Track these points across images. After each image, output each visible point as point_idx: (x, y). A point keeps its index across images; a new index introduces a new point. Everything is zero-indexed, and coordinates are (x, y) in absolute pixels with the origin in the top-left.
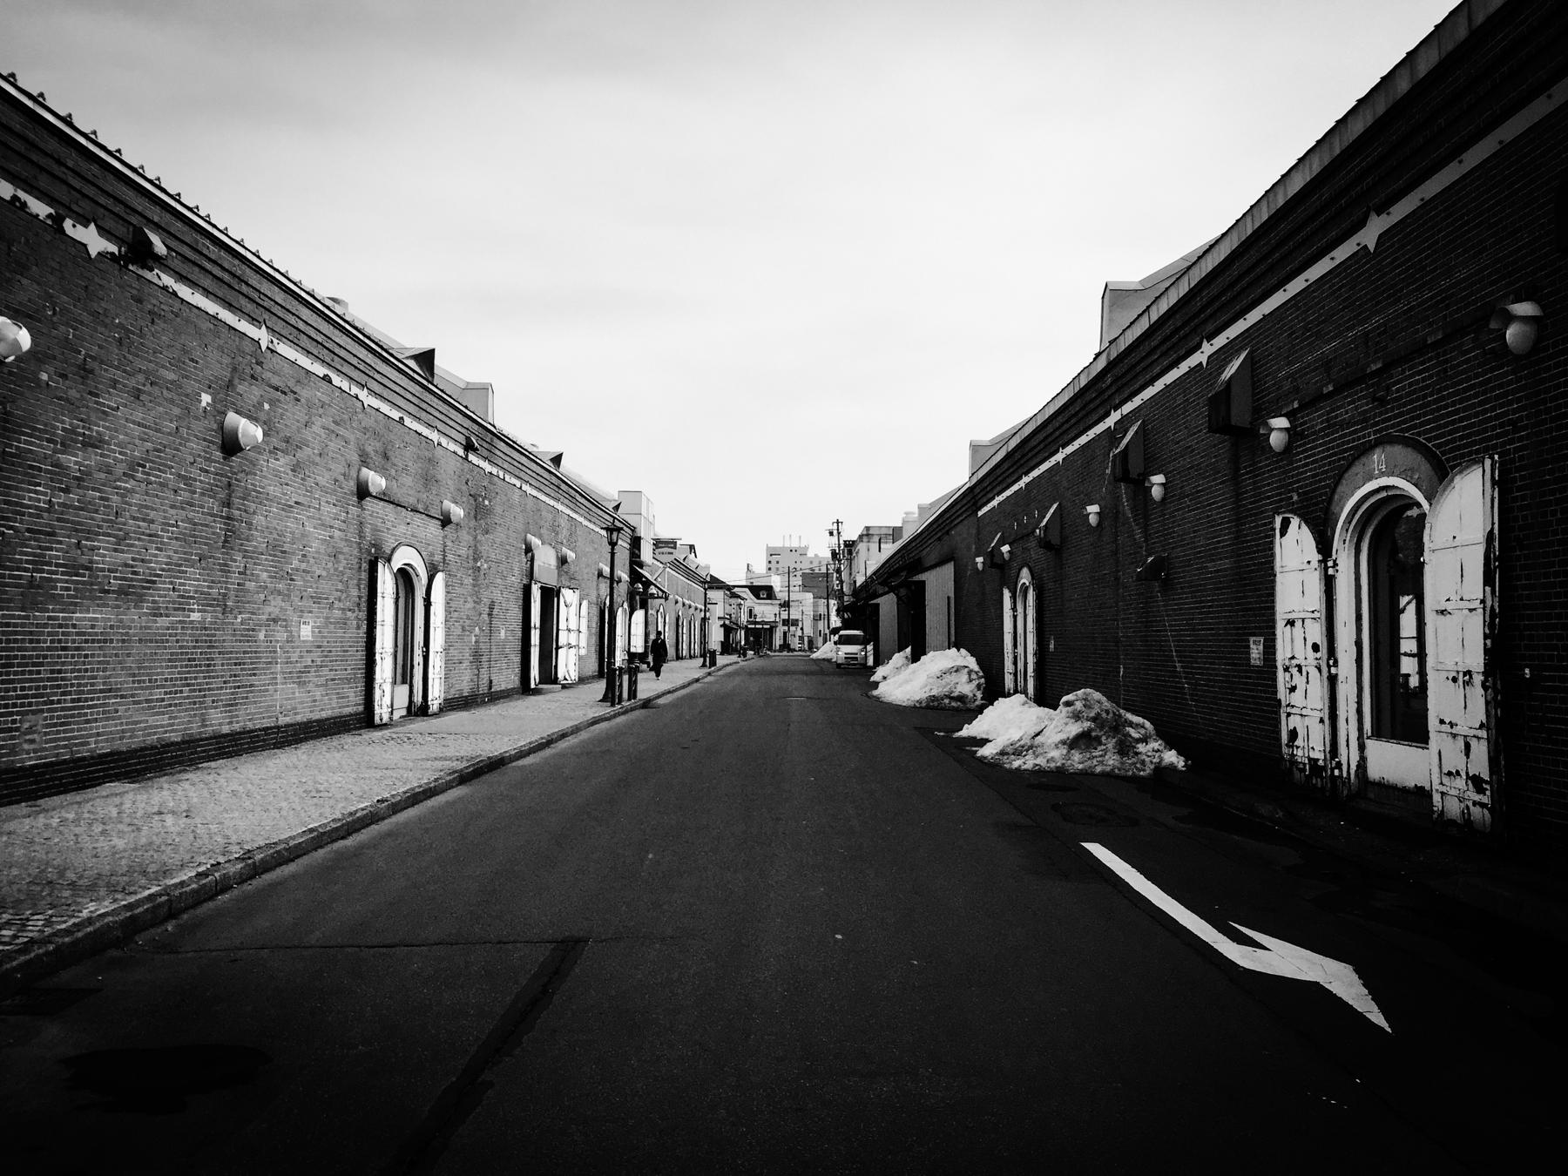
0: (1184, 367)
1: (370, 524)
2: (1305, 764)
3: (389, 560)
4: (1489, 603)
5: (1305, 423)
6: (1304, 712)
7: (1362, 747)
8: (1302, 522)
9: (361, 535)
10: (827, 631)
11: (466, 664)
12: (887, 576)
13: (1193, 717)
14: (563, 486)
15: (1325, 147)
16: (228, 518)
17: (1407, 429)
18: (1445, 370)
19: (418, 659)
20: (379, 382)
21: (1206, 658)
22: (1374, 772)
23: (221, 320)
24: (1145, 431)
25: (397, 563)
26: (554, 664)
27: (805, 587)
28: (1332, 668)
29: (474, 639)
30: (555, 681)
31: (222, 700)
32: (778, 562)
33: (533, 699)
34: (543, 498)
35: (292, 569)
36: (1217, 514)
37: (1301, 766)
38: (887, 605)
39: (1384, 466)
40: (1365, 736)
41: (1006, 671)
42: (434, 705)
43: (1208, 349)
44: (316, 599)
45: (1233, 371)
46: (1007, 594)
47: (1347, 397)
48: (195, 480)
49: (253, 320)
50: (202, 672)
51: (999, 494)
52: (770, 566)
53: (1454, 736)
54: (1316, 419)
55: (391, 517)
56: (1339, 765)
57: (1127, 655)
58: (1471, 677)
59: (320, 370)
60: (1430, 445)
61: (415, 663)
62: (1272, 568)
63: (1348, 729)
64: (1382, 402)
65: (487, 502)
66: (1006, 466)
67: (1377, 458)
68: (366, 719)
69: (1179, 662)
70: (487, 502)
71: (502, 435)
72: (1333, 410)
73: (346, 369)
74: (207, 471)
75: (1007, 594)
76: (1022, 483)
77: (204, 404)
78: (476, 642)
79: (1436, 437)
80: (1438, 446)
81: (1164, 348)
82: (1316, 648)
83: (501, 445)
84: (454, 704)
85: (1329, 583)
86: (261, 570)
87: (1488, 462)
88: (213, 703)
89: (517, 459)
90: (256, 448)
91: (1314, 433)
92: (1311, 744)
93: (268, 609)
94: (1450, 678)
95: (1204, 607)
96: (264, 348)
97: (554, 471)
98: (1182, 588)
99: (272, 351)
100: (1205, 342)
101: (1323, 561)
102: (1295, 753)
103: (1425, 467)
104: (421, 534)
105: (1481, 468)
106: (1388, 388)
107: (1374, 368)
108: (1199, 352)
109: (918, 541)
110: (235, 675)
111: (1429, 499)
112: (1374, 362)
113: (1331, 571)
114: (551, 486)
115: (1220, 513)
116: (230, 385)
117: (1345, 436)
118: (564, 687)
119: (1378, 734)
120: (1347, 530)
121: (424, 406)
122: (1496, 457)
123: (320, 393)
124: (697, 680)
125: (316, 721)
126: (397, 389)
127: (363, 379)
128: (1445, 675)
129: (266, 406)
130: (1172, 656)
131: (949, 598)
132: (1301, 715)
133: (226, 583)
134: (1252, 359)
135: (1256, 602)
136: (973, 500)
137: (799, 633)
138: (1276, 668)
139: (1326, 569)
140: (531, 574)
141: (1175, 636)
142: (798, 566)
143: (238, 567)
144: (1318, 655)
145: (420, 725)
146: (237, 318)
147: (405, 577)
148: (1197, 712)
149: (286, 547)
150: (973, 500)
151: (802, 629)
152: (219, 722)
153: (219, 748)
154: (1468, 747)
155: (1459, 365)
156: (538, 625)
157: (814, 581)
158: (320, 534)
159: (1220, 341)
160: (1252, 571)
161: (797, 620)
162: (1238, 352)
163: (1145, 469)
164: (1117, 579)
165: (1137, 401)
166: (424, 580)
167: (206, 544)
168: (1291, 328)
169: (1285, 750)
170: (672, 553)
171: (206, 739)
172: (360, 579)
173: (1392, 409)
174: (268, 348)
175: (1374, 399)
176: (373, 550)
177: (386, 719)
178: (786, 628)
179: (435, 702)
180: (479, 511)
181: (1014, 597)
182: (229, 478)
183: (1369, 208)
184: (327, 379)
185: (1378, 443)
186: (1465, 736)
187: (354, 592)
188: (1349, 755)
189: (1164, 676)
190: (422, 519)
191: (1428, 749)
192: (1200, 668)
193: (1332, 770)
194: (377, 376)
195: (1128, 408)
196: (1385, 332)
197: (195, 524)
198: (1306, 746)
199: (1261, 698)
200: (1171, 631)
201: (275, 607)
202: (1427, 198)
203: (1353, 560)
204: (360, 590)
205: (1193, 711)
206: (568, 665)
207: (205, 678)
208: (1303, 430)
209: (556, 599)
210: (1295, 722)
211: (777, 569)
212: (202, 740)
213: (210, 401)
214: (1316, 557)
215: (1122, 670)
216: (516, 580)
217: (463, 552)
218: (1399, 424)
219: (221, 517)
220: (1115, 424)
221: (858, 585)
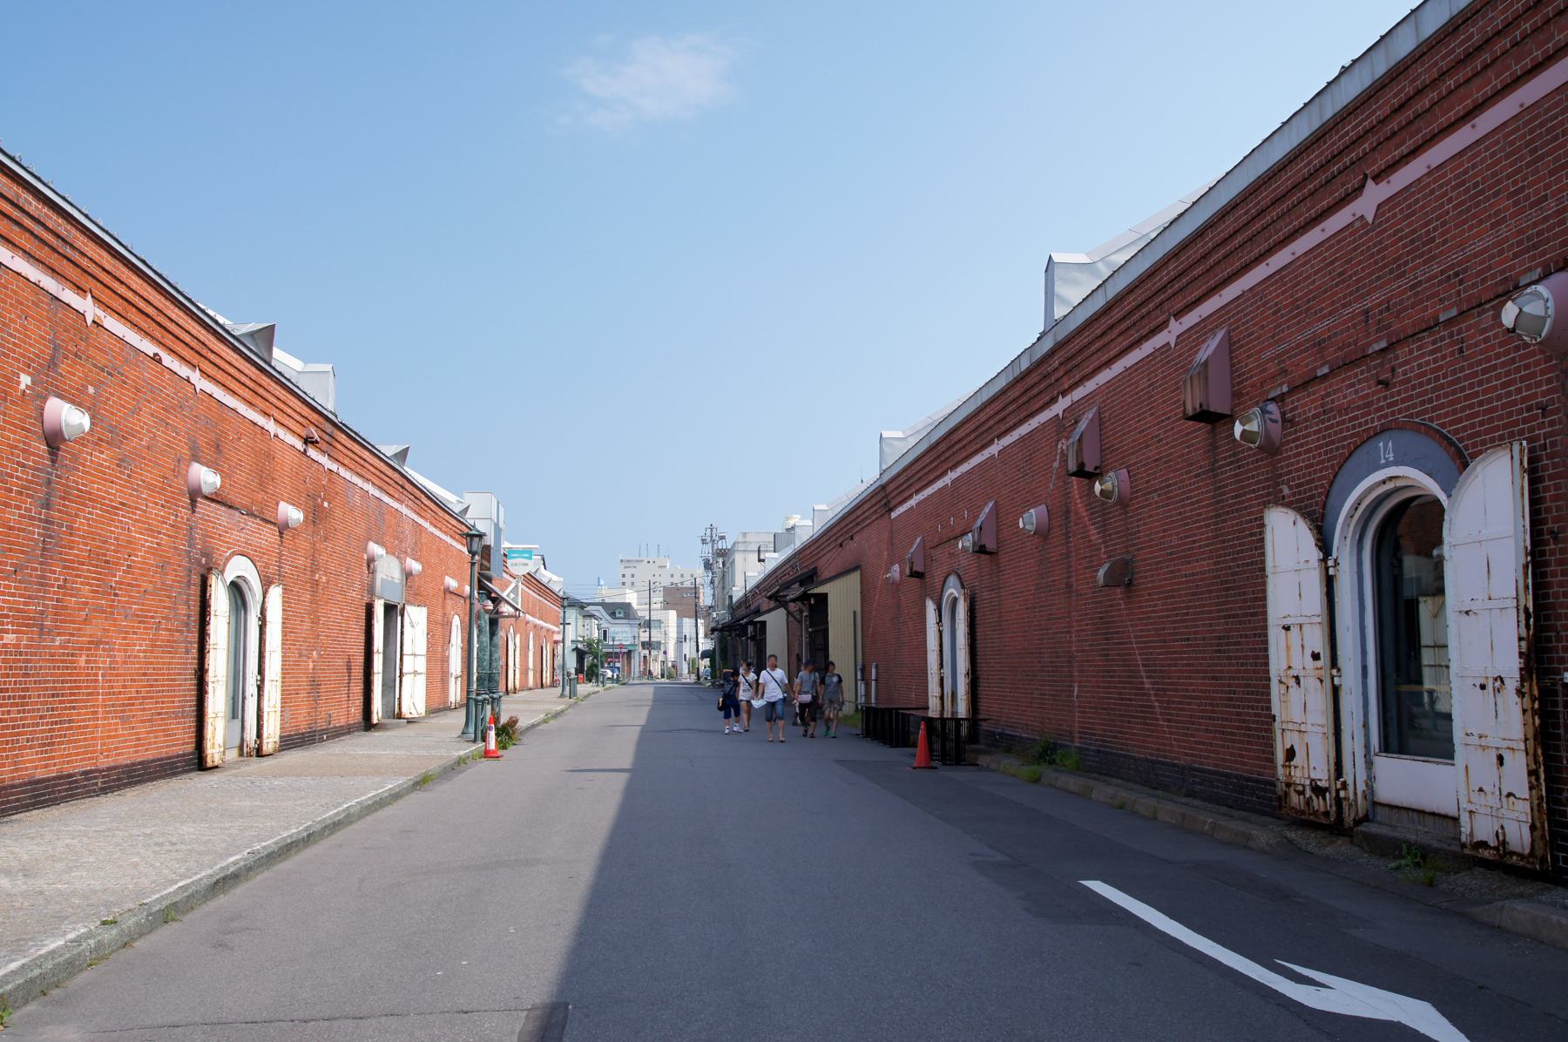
0: (1148, 348)
1: (201, 529)
2: (1304, 786)
3: (222, 572)
4: (1522, 603)
5: (1295, 408)
6: (1303, 728)
7: (1369, 764)
8: (1298, 517)
9: (191, 541)
10: (694, 655)
11: (303, 694)
12: (775, 589)
13: (1167, 738)
14: (408, 486)
15: (1314, 108)
16: (46, 522)
17: (1418, 414)
18: (1461, 351)
19: (251, 689)
20: (212, 362)
21: (1180, 671)
22: (1385, 793)
23: (42, 289)
24: (1100, 419)
25: (230, 575)
26: (397, 696)
27: (667, 605)
28: (1335, 679)
29: (311, 665)
30: (400, 716)
31: (38, 739)
32: (633, 576)
33: (375, 735)
34: (386, 499)
35: (116, 582)
36: (1191, 510)
37: (1300, 788)
38: (776, 623)
39: (1392, 455)
40: (1372, 753)
41: (930, 694)
42: (270, 743)
43: (1176, 328)
44: (141, 619)
45: (1210, 351)
46: (930, 607)
47: (1343, 381)
48: (11, 476)
49: (80, 290)
50: (16, 705)
51: (917, 492)
52: (624, 580)
53: (1484, 748)
54: (1305, 405)
55: (224, 520)
57: (1082, 671)
58: (1502, 682)
59: (149, 348)
60: (1444, 431)
61: (248, 694)
62: (1263, 569)
63: (1353, 745)
64: (1386, 384)
65: (326, 504)
66: (927, 460)
67: (1385, 447)
68: (199, 762)
69: (1148, 677)
70: (326, 504)
71: (344, 425)
72: (1328, 395)
73: (179, 348)
74: (23, 466)
75: (930, 607)
76: (948, 479)
77: (23, 387)
78: (314, 669)
79: (1452, 423)
80: (1456, 432)
81: (1123, 326)
82: (1316, 657)
83: (342, 438)
84: (289, 742)
85: (1329, 582)
86: (82, 583)
87: (1516, 447)
88: (28, 742)
89: (359, 453)
90: (82, 440)
91: (1306, 420)
92: (1314, 765)
93: (88, 630)
94: (1478, 685)
95: (1177, 615)
96: (89, 322)
97: (397, 467)
98: (1149, 594)
99: (99, 325)
100: (1172, 320)
101: (1324, 560)
102: (1292, 774)
103: (1441, 455)
104: (254, 540)
105: (1509, 456)
106: (1393, 370)
107: (1377, 347)
108: (1166, 330)
109: (813, 548)
110: (53, 709)
111: (1448, 490)
112: (1377, 340)
113: (1331, 571)
114: (396, 486)
115: (1196, 509)
116: (52, 364)
117: (1343, 422)
118: (410, 721)
119: (1386, 748)
120: (1349, 525)
121: (261, 391)
122: (1524, 443)
123: (148, 372)
124: (557, 715)
125: (141, 763)
126: (232, 371)
127: (195, 359)
128: (1470, 682)
129: (91, 390)
130: (1139, 671)
131: (855, 612)
132: (1300, 731)
133: (44, 598)
134: (1230, 338)
135: (1240, 608)
136: (885, 500)
137: (661, 657)
138: (1269, 679)
139: (1327, 569)
140: (371, 590)
141: (1142, 648)
142: (657, 579)
143: (57, 580)
144: (1319, 663)
145: (256, 764)
146: (61, 287)
147: (237, 590)
148: (1170, 733)
149: (110, 556)
150: (885, 500)
151: (665, 653)
152: (35, 766)
153: (35, 796)
154: (1500, 759)
155: (1476, 345)
156: (381, 650)
157: (681, 599)
158: (147, 541)
159: (1191, 319)
160: (1236, 573)
161: (659, 643)
162: (1213, 331)
163: (1102, 462)
164: (1069, 586)
165: (1090, 386)
166: (259, 597)
167: (23, 552)
168: (1276, 305)
169: (1280, 771)
170: (526, 565)
171: (20, 785)
172: (189, 595)
173: (1399, 393)
174: (94, 322)
175: (1380, 382)
176: (204, 560)
177: (217, 761)
178: (647, 652)
179: (271, 740)
180: (316, 515)
181: (939, 610)
182: (48, 473)
183: (1366, 177)
184: (156, 359)
185: (1384, 430)
186: (1497, 748)
187: (183, 610)
188: (1354, 771)
189: (1129, 694)
190: (257, 524)
191: (1453, 765)
192: (1173, 684)
193: (1337, 791)
194: (212, 357)
195: (1078, 394)
196: (1388, 309)
197: (11, 528)
198: (1306, 766)
199: (1247, 715)
200: (1137, 643)
201: (95, 629)
202: (1433, 166)
203: (1355, 558)
204: (189, 607)
205: (1164, 732)
206: (414, 698)
207: (19, 712)
208: (1294, 417)
209: (399, 618)
210: (1291, 739)
211: (633, 584)
212: (13, 786)
213: (29, 384)
214: (1315, 554)
215: (1076, 689)
216: (357, 596)
217: (301, 562)
218: (1407, 409)
219: (40, 520)
220: (1064, 411)
221: (734, 600)
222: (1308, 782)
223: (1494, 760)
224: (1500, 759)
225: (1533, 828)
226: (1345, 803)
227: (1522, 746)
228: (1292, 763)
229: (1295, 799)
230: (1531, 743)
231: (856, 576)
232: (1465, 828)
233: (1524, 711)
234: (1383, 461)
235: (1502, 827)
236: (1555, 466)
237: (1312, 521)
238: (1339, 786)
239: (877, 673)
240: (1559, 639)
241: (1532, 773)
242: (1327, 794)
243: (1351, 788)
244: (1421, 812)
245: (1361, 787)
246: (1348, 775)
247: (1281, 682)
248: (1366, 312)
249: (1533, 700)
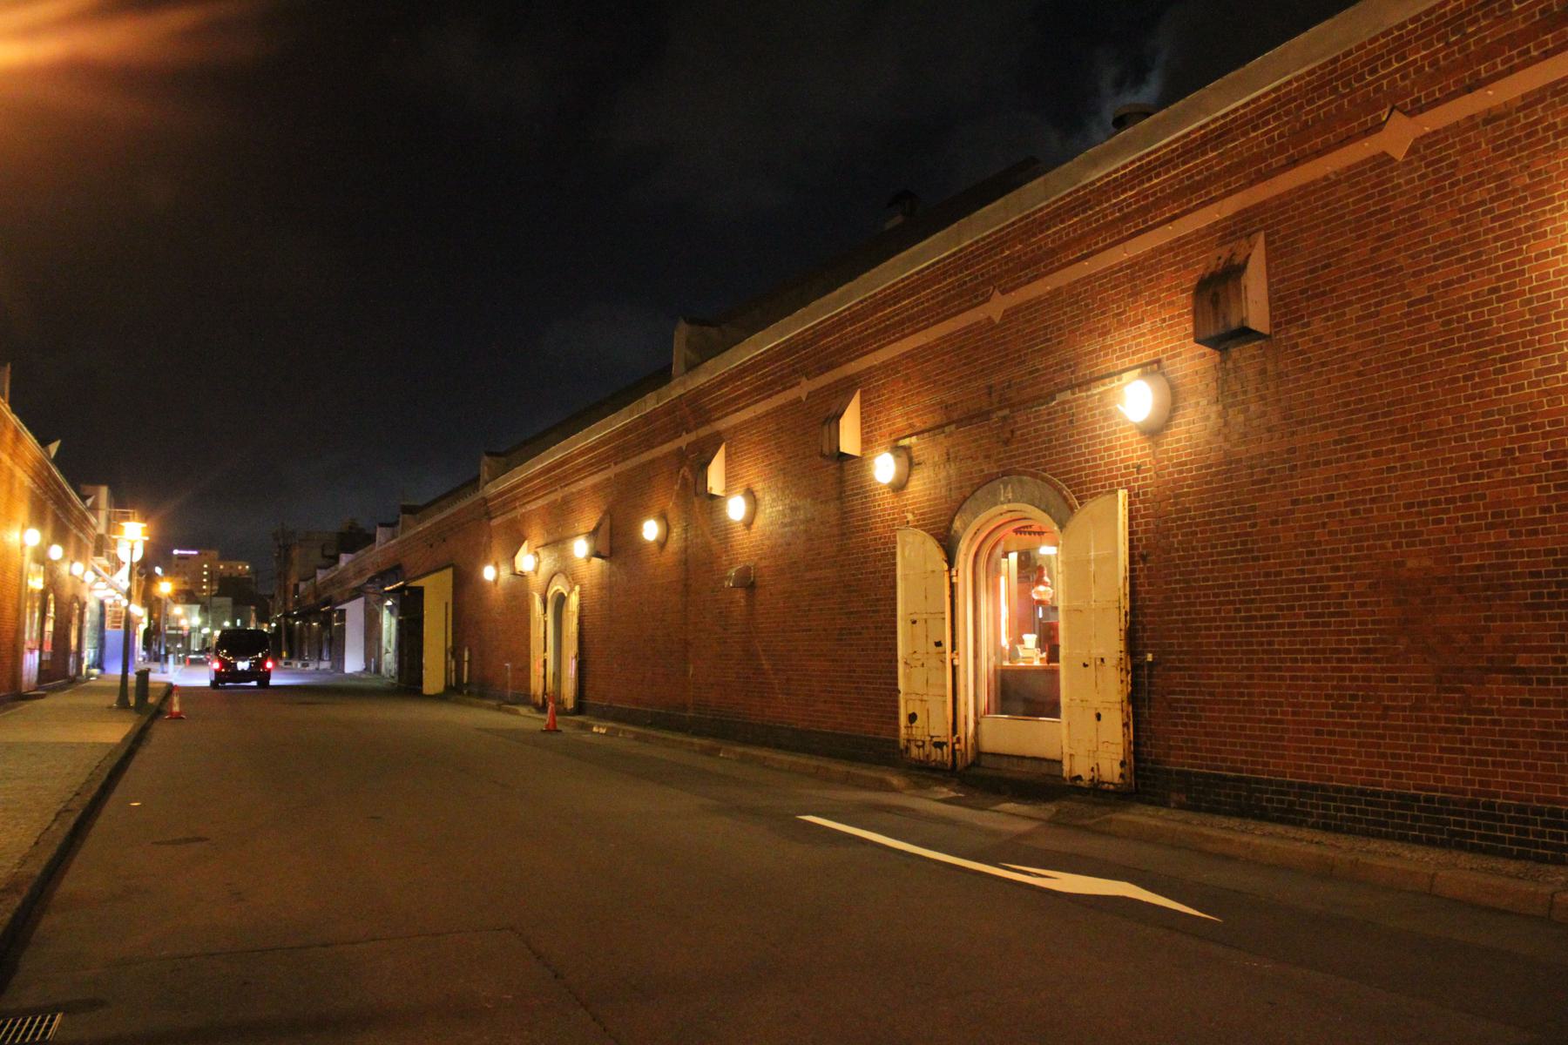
2: (924, 742)
6: (925, 698)
37: (920, 743)
56: (958, 740)
106: (1012, 432)
131: (447, 604)
154: (1099, 717)
169: (903, 731)
198: (926, 726)
220: (688, 445)
222: (928, 738)
223: (1094, 718)
224: (1099, 717)
225: (1123, 764)
226: (958, 753)
227: (1119, 706)
228: (914, 725)
229: (915, 752)
230: (1125, 704)
231: (449, 572)
232: (1066, 767)
233: (1122, 681)
234: (1002, 499)
235: (1097, 765)
236: (1145, 509)
237: (939, 541)
238: (955, 740)
239: (470, 655)
240: (1144, 630)
241: (1125, 725)
242: (945, 747)
243: (963, 741)
244: (1023, 757)
245: (970, 741)
246: (961, 732)
247: (906, 663)
248: (990, 387)
249: (1128, 673)
